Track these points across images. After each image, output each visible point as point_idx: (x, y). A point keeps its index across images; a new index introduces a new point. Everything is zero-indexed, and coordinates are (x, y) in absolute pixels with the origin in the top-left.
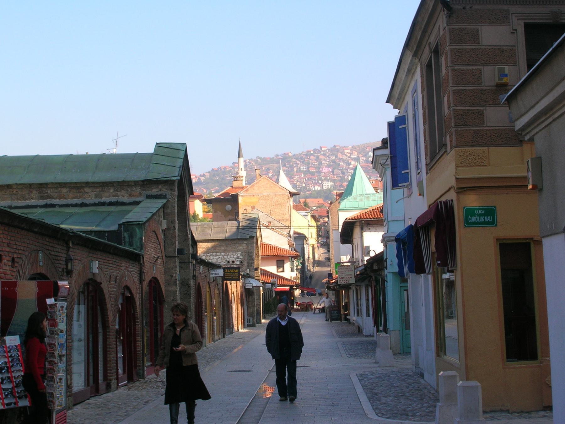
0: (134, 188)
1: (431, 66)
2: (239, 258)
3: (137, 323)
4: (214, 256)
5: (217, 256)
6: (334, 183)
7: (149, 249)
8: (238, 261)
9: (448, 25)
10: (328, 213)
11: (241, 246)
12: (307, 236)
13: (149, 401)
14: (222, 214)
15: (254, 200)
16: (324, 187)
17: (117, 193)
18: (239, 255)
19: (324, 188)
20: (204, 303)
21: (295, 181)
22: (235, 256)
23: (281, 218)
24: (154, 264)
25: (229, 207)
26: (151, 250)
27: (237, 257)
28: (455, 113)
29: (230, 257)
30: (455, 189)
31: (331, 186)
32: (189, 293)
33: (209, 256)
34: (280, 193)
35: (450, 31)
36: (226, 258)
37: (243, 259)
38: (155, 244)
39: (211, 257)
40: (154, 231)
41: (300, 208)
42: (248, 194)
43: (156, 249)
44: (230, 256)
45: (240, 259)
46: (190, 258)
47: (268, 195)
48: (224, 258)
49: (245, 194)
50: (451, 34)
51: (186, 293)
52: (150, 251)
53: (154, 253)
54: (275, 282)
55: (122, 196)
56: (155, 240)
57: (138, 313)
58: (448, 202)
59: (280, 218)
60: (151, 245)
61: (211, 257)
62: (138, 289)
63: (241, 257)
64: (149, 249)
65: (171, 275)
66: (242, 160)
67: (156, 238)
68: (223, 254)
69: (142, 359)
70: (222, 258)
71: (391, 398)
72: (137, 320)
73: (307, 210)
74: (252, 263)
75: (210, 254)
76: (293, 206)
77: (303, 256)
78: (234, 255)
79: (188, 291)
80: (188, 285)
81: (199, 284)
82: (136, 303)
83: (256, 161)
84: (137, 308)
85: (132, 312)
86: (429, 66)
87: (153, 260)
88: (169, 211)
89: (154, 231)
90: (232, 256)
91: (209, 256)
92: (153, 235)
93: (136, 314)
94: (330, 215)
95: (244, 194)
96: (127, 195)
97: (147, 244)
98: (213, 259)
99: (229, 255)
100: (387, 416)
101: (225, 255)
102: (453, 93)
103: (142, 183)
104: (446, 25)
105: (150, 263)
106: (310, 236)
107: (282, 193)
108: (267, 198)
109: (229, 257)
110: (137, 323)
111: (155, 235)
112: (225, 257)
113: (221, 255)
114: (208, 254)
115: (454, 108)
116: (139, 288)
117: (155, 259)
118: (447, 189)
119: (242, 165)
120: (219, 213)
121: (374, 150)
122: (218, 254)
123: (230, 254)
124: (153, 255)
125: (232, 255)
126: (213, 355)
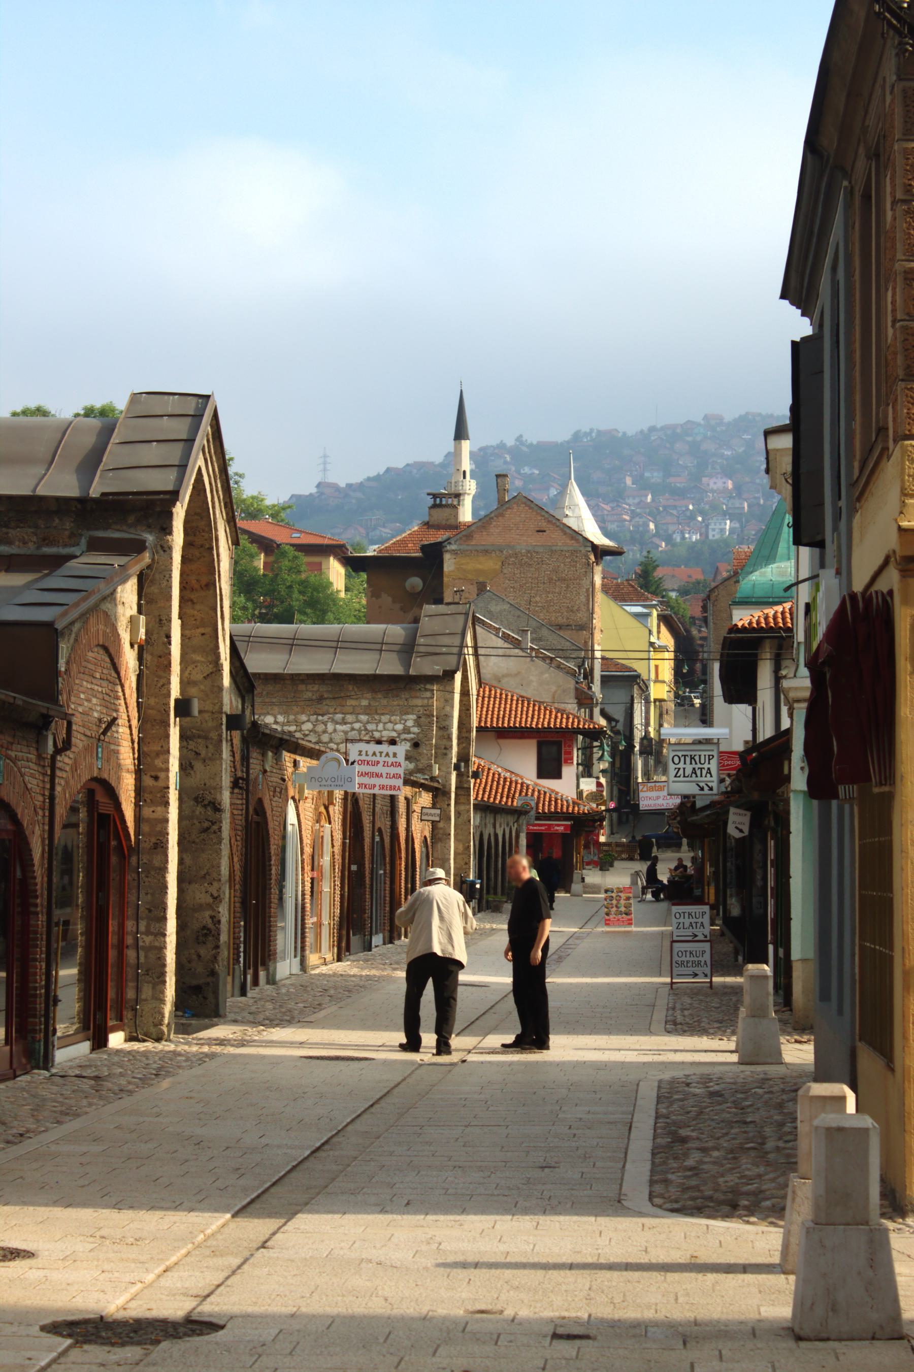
0: (57, 521)
1: (870, 197)
2: (409, 733)
3: (32, 909)
4: (337, 723)
5: (346, 723)
6: (740, 522)
7: (82, 696)
8: (405, 739)
9: (899, 79)
10: (706, 612)
11: (417, 697)
12: (644, 676)
13: (28, 1131)
14: (394, 602)
15: (489, 564)
16: (711, 533)
17: (7, 533)
18: (410, 723)
19: (711, 537)
20: (273, 858)
21: (627, 514)
22: (399, 727)
23: (565, 620)
24: (99, 740)
25: (415, 582)
26: (89, 701)
27: (404, 729)
28: (906, 340)
29: (385, 729)
30: (898, 558)
31: (732, 531)
32: (215, 827)
33: (325, 724)
34: (565, 548)
35: (905, 97)
36: (372, 731)
37: (421, 735)
38: (105, 683)
39: (330, 727)
40: (106, 649)
41: (628, 594)
42: (470, 548)
43: (107, 698)
44: (385, 723)
45: (412, 736)
46: (224, 727)
47: (529, 552)
48: (366, 729)
49: (464, 547)
50: (907, 106)
51: (208, 829)
52: (86, 704)
53: (98, 708)
54: (528, 804)
55: (19, 541)
56: (105, 671)
57: (39, 880)
58: (874, 595)
59: (561, 620)
60: (89, 686)
61: (330, 727)
62: (41, 812)
63: (416, 730)
64: (82, 696)
65: (153, 774)
66: (466, 445)
67: (109, 665)
68: (363, 718)
69: (43, 1012)
70: (359, 731)
71: (715, 1154)
72: (32, 901)
73: (647, 599)
74: (446, 748)
75: (326, 718)
76: (603, 585)
77: (627, 734)
78: (396, 724)
79: (213, 823)
80: (214, 804)
81: (260, 801)
82: (31, 850)
83: (510, 451)
84: (33, 865)
85: (19, 874)
86: (866, 197)
87: (95, 728)
88: (154, 589)
89: (106, 649)
90: (390, 726)
91: (325, 724)
92: (99, 657)
93: (32, 881)
94: (710, 619)
95: (461, 547)
96: (34, 539)
97: (77, 681)
98: (335, 730)
99: (380, 721)
100: (676, 1206)
101: (368, 722)
102: (906, 279)
103: (79, 506)
104: (894, 78)
105: (83, 738)
106: (653, 676)
107: (571, 548)
108: (525, 559)
109: (380, 727)
110: (32, 909)
111: (107, 659)
112: (370, 727)
113: (358, 721)
114: (320, 718)
115: (905, 323)
116: (43, 809)
117: (104, 726)
118: (880, 561)
119: (466, 465)
120: (386, 599)
121: (768, 433)
122: (350, 718)
123: (385, 718)
124: (96, 715)
125: (390, 722)
126: (283, 1010)
